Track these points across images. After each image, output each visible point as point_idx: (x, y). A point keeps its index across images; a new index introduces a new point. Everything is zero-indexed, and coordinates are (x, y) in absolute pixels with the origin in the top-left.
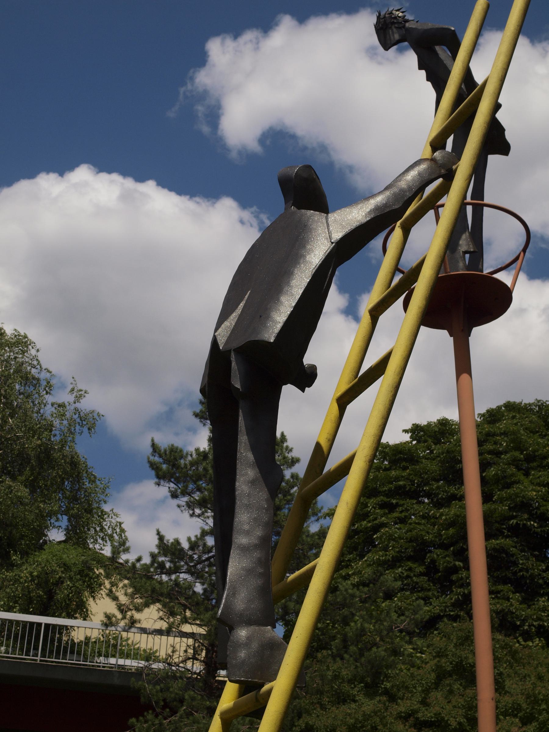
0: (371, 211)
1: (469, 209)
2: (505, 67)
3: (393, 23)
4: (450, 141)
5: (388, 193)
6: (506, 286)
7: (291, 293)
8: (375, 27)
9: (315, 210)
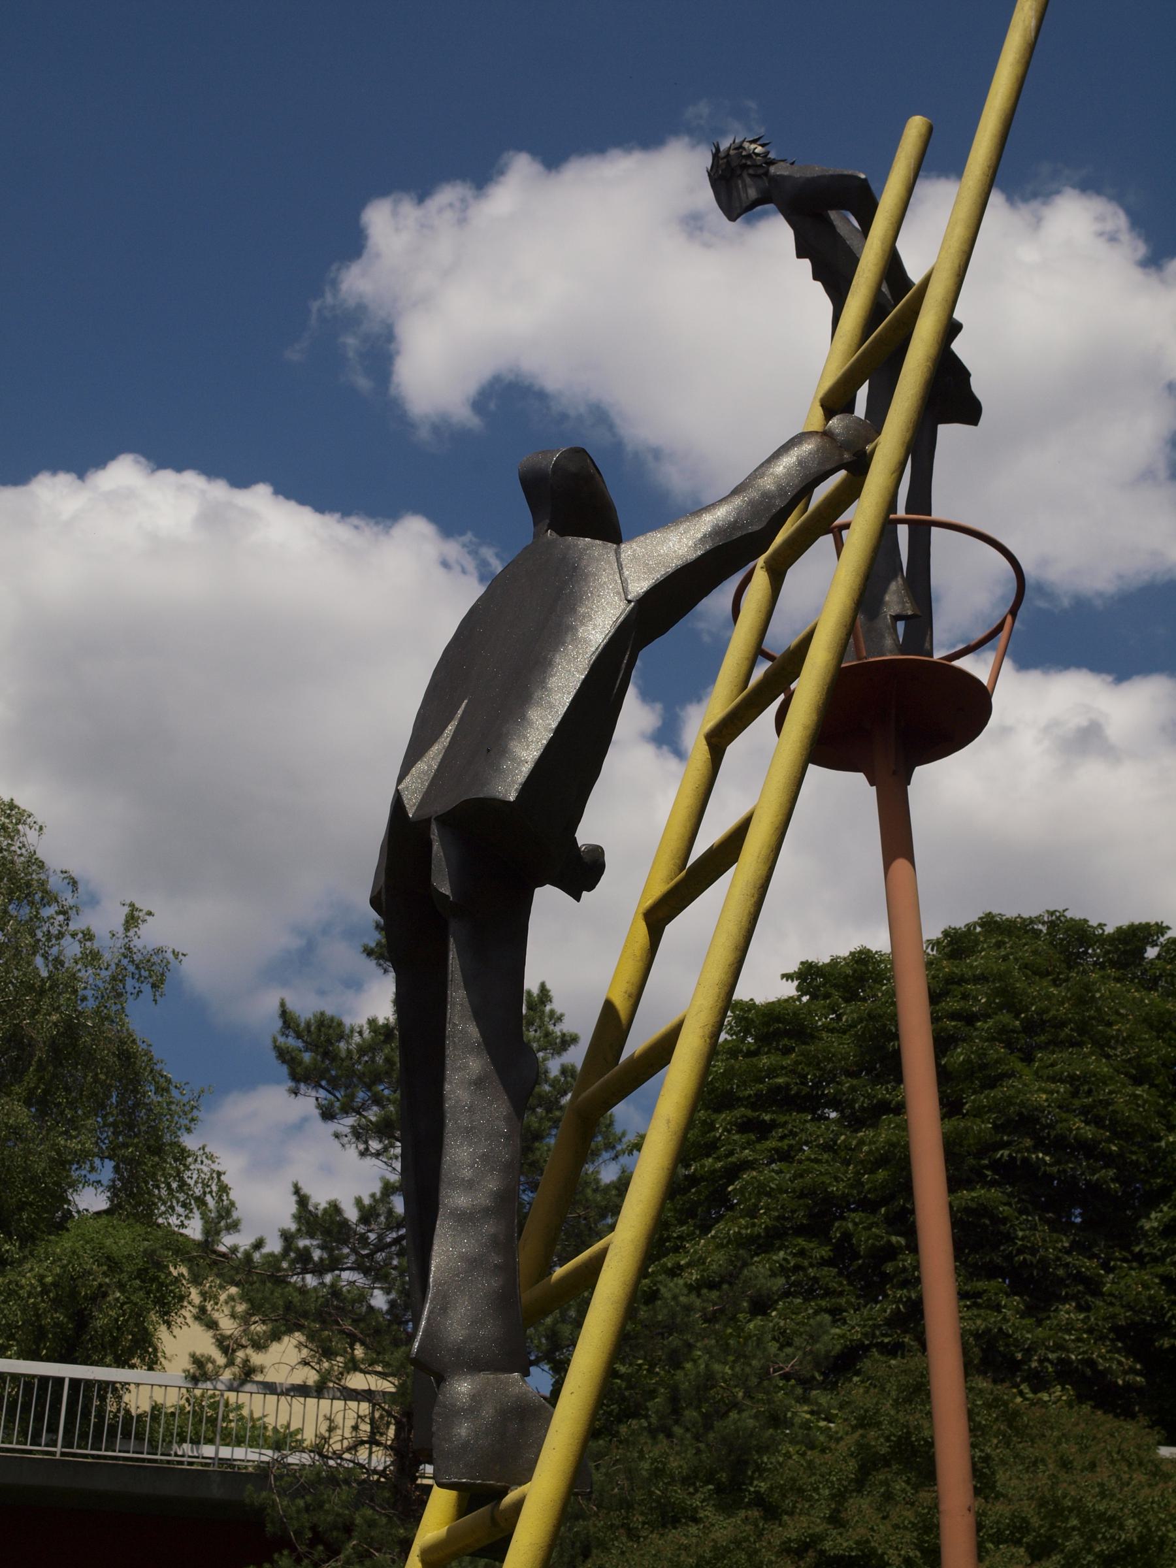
0: (705, 536)
1: (903, 531)
2: (966, 247)
4: (863, 393)
5: (738, 501)
7: (549, 702)
8: (709, 175)
9: (594, 537)
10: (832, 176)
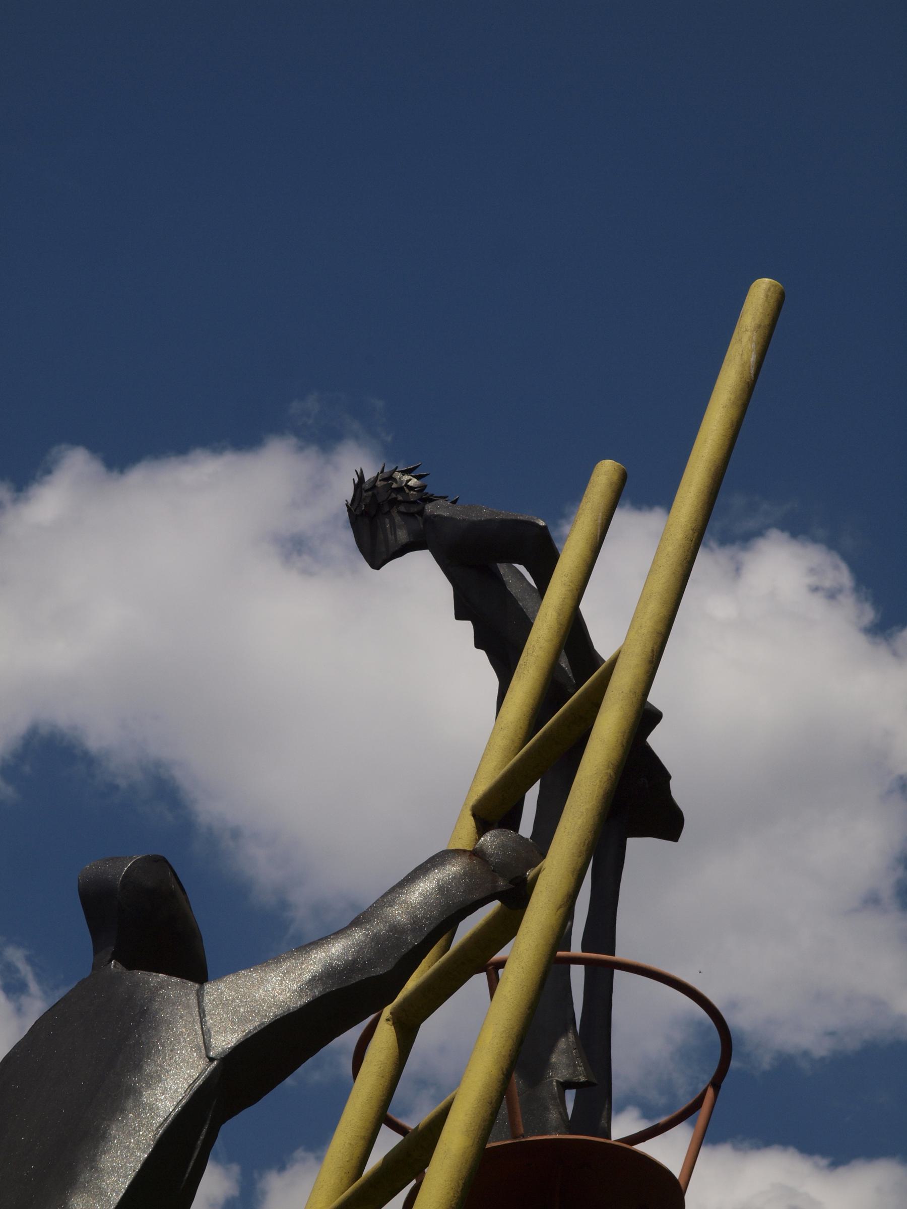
1: (577, 974)
2: (661, 628)
3: (394, 503)
4: (532, 796)
5: (358, 935)
7: (99, 1188)
8: (349, 510)
9: (171, 972)
10: (503, 522)
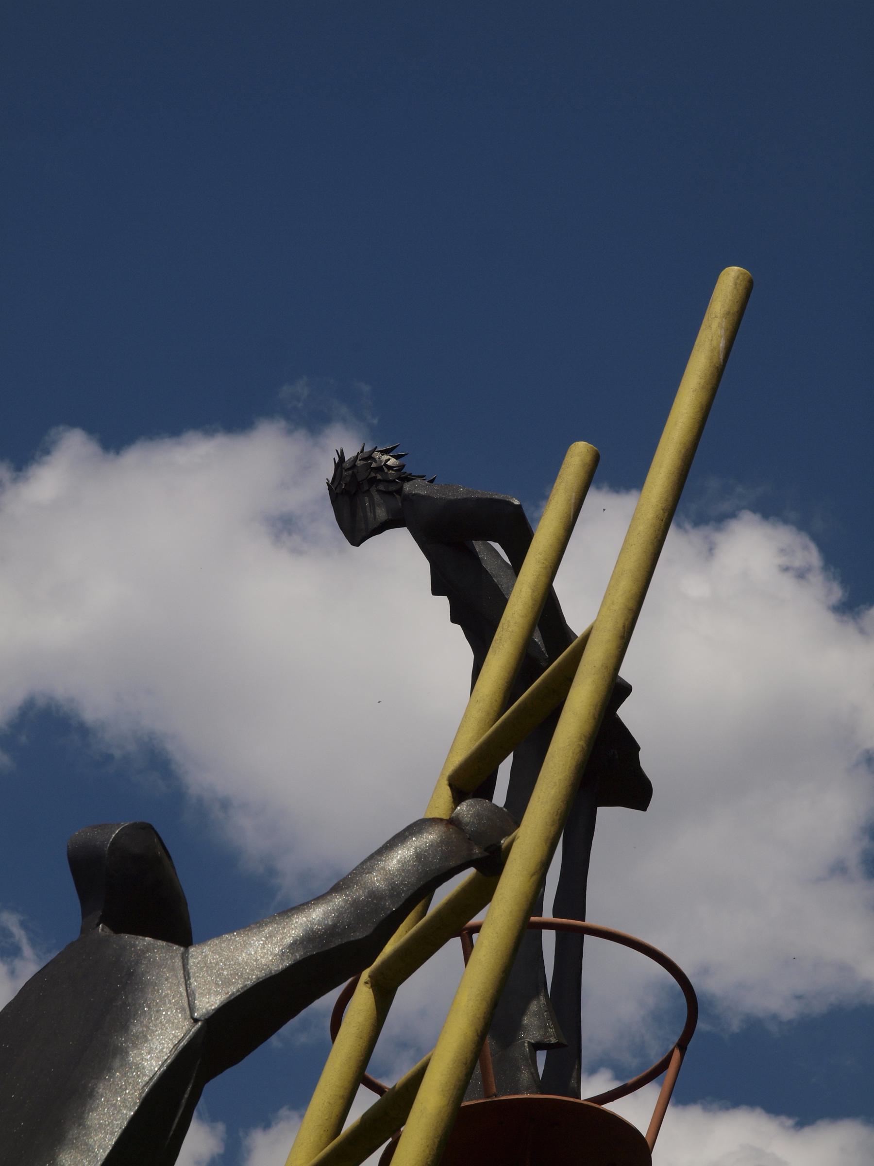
0: (295, 942)
1: (549, 938)
2: (632, 604)
3: (373, 481)
5: (338, 900)
6: (633, 1131)
7: (86, 1144)
8: (330, 488)
9: (156, 937)
10: (478, 500)
